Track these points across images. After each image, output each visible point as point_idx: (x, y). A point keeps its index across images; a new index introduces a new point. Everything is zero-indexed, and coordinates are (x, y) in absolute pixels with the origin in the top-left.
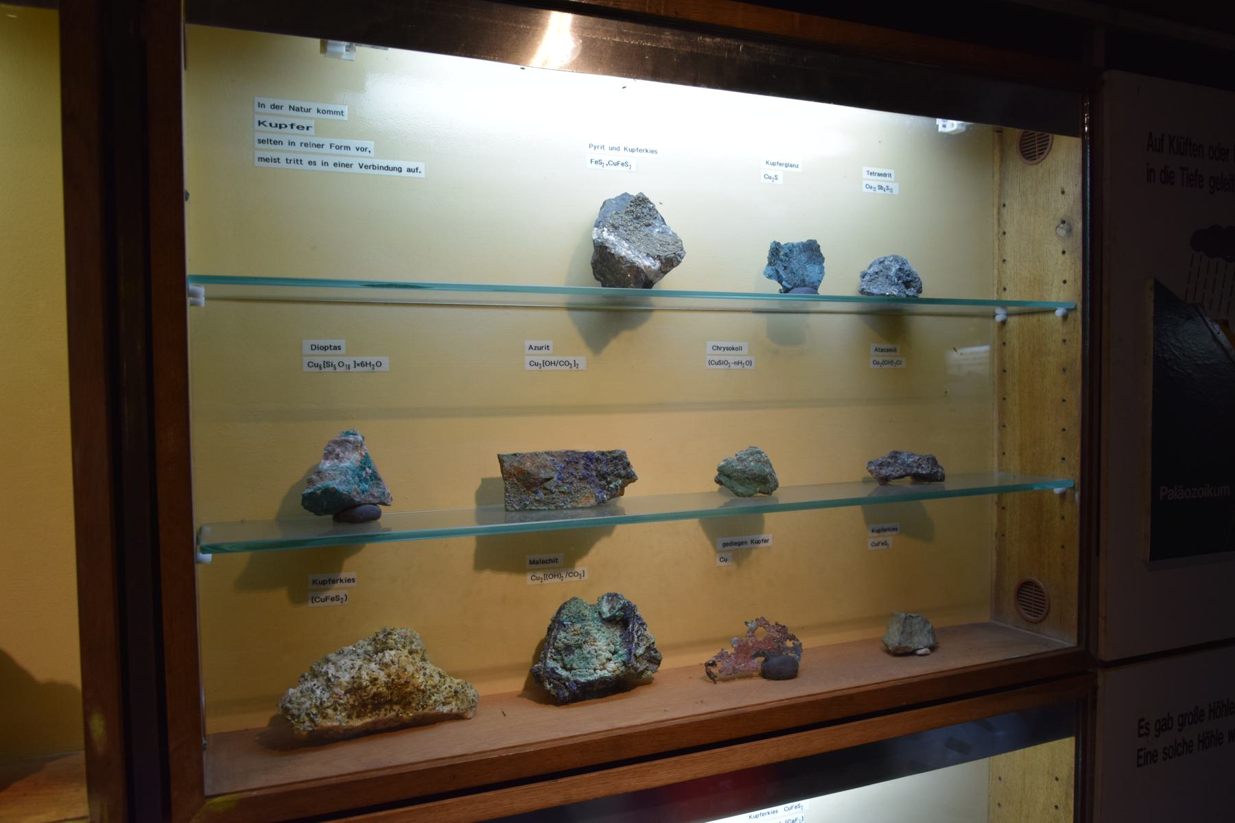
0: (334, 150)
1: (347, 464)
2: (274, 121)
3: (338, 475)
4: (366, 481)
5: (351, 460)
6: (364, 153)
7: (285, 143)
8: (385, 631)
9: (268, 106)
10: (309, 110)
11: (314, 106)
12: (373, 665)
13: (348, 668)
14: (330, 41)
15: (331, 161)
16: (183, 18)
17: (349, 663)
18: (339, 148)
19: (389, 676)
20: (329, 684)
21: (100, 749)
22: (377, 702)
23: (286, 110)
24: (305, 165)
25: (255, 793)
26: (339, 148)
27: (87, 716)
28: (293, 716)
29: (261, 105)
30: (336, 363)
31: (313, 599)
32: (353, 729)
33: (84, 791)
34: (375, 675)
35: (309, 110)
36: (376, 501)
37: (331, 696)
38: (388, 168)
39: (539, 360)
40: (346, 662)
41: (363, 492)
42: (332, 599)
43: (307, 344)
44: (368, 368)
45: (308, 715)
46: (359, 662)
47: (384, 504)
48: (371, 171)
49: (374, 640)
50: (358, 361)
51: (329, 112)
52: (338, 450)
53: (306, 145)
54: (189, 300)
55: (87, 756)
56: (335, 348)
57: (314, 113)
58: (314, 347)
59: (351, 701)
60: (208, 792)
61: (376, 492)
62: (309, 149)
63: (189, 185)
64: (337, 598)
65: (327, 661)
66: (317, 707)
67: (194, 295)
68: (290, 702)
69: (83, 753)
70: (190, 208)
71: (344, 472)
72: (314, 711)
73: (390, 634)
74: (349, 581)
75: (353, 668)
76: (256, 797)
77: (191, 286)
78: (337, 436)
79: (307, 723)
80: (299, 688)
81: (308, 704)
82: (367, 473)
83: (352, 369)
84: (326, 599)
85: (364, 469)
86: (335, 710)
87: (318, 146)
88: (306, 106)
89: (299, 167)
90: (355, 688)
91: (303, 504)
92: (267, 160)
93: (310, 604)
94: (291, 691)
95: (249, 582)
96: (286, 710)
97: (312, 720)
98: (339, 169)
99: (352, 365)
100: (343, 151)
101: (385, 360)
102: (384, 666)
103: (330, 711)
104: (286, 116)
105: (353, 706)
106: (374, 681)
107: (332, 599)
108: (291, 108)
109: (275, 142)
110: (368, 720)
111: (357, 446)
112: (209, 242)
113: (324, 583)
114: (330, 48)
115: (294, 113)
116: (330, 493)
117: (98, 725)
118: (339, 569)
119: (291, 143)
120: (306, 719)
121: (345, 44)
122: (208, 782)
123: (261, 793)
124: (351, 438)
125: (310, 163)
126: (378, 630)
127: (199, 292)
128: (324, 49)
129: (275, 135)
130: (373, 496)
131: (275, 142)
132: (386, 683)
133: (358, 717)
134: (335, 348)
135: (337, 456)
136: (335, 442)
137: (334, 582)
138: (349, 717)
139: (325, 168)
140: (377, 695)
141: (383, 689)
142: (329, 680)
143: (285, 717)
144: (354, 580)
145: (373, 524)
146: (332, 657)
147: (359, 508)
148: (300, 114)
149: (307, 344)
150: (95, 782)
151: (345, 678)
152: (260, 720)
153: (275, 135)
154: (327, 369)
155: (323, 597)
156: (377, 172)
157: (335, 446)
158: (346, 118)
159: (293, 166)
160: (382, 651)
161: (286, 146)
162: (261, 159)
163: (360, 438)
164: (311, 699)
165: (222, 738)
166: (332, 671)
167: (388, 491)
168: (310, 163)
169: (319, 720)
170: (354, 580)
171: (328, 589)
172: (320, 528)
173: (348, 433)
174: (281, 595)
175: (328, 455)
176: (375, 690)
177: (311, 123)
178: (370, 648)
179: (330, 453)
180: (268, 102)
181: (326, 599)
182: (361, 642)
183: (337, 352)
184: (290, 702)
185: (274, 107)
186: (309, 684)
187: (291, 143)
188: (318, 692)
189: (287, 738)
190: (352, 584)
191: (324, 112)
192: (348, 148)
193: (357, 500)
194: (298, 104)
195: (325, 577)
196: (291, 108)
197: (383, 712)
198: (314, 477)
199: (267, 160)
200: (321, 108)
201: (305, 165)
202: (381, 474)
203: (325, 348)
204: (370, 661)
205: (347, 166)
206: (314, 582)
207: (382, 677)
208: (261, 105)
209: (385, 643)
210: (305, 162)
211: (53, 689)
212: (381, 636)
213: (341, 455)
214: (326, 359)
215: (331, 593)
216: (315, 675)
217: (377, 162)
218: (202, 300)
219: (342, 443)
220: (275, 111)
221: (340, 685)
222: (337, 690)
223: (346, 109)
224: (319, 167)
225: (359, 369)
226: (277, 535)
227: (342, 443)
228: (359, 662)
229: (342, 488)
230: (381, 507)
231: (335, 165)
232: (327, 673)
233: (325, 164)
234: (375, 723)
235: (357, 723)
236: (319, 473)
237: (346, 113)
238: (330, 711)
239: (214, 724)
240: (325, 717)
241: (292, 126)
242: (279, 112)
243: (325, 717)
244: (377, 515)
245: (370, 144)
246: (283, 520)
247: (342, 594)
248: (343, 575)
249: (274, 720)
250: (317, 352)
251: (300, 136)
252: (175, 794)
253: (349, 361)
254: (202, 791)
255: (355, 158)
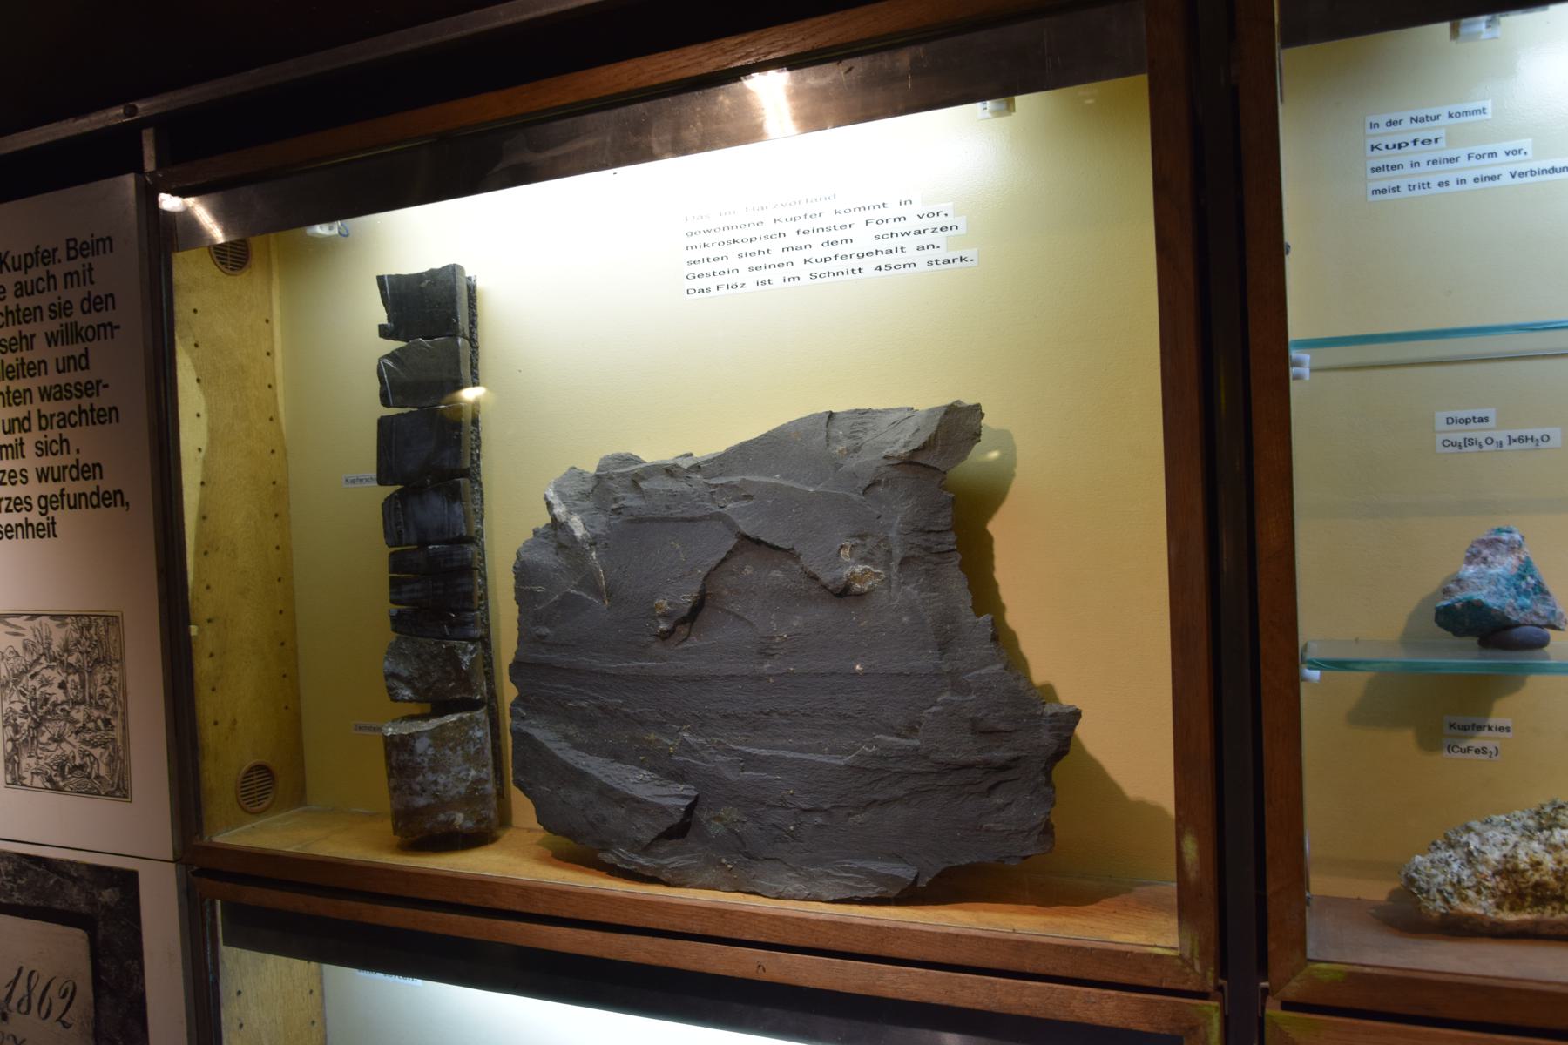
0: (1473, 161)
1: (1498, 570)
2: (1390, 141)
3: (1488, 584)
4: (1526, 593)
5: (1505, 565)
6: (1518, 157)
7: (1407, 165)
8: (1554, 803)
9: (1383, 124)
10: (1437, 117)
11: (1443, 111)
12: (1535, 845)
13: (1495, 843)
14: (1464, 21)
15: (1470, 176)
16: (1278, 44)
17: (1500, 837)
18: (1481, 156)
19: (1560, 862)
20: (1470, 859)
21: (1192, 875)
22: (1540, 895)
23: (1406, 124)
24: (1435, 189)
25: (1368, 970)
26: (1481, 156)
27: (1179, 835)
28: (1420, 889)
29: (1374, 125)
30: (1537, 436)
31: (1450, 748)
32: (1503, 924)
33: (1174, 923)
34: (1538, 857)
35: (1437, 117)
36: (1542, 622)
37: (1474, 874)
38: (1554, 170)
39: (1459, 438)
40: (1495, 835)
41: (1522, 608)
42: (1477, 751)
43: (1440, 417)
44: (1530, 444)
45: (1440, 892)
46: (1513, 838)
47: (1554, 627)
48: (1529, 179)
49: (1538, 813)
50: (1515, 435)
51: (1466, 113)
52: (1485, 552)
53: (1435, 162)
54: (1293, 370)
55: (1179, 888)
56: (1481, 420)
57: (1444, 120)
58: (1451, 421)
59: (1502, 886)
60: (1310, 955)
61: (1542, 609)
62: (1439, 167)
63: (1290, 236)
64: (1484, 750)
65: (1469, 829)
66: (1453, 885)
67: (1298, 364)
68: (1416, 871)
69: (1175, 885)
70: (1292, 264)
71: (1494, 581)
72: (1449, 889)
73: (1562, 807)
74: (1501, 729)
75: (1505, 843)
76: (1368, 974)
77: (1294, 354)
78: (1484, 535)
79: (1439, 903)
80: (1431, 856)
81: (1441, 878)
82: (1528, 582)
83: (1505, 446)
84: (1468, 750)
85: (1523, 578)
86: (1479, 893)
87: (1451, 160)
88: (1432, 112)
89: (1427, 191)
90: (1508, 870)
91: (1437, 619)
92: (1383, 191)
93: (1445, 753)
94: (1418, 858)
95: (1368, 714)
96: (1411, 881)
97: (1445, 900)
98: (1481, 185)
99: (1505, 441)
100: (1487, 161)
101: (1556, 433)
102: (1553, 848)
103: (1471, 893)
104: (1408, 131)
105: (1505, 894)
106: (1536, 865)
107: (1477, 751)
108: (1414, 120)
109: (1394, 167)
110: (1526, 916)
111: (1513, 548)
112: (1312, 302)
113: (1465, 728)
114: (1463, 31)
115: (1419, 125)
116: (1474, 607)
117: (1190, 847)
118: (1487, 712)
119: (1415, 164)
120: (1438, 896)
121: (1484, 19)
122: (1311, 945)
123: (1376, 971)
124: (1505, 537)
125: (1440, 184)
126: (1544, 801)
127: (1303, 363)
128: (1455, 33)
129: (1393, 158)
130: (1537, 614)
131: (1394, 167)
132: (1555, 872)
133: (1512, 909)
134: (1481, 420)
135: (1485, 561)
136: (1482, 542)
137: (1480, 728)
138: (1499, 906)
139: (1463, 187)
140: (1538, 885)
141: (1550, 879)
142: (1470, 853)
143: (1410, 889)
144: (1508, 730)
145: (1537, 652)
146: (1476, 825)
147: (1516, 630)
148: (1426, 124)
149: (1440, 417)
150: (1186, 910)
151: (1495, 855)
152: (1378, 891)
153: (1393, 158)
154: (1470, 448)
155: (1464, 746)
156: (1537, 178)
157: (1481, 548)
158: (1489, 116)
159: (1417, 192)
160: (1550, 828)
161: (1407, 169)
162: (1375, 192)
163: (1517, 537)
164: (1445, 873)
165: (1329, 902)
166: (1474, 843)
167: (1560, 610)
168: (1440, 184)
169: (1455, 902)
170: (1508, 730)
171: (1466, 738)
172: (1464, 656)
173: (1500, 531)
174: (1408, 736)
175: (1471, 558)
176: (1537, 877)
177: (1442, 133)
178: (1531, 823)
179: (1475, 556)
180: (1382, 119)
181: (1468, 750)
182: (1518, 813)
183: (1483, 425)
184: (1416, 871)
185: (1391, 123)
186: (1443, 854)
187: (1415, 164)
188: (1455, 866)
189: (1409, 916)
190: (1505, 734)
191: (1458, 115)
192: (1493, 154)
193: (1514, 618)
194: (1421, 113)
195: (1469, 720)
196: (1414, 120)
197: (1549, 910)
198: (1452, 586)
199: (1383, 191)
200: (1453, 111)
201: (1435, 189)
202: (1549, 586)
203: (1466, 421)
204: (1531, 839)
205: (1492, 178)
206: (1451, 726)
207: (1549, 862)
208: (1374, 125)
209: (1555, 819)
210: (1434, 184)
211: (1142, 809)
212: (1548, 810)
213: (1490, 559)
214: (1469, 435)
215: (1475, 743)
216: (1451, 845)
217: (1535, 166)
218: (1306, 371)
219: (1492, 543)
220: (1393, 128)
221: (1486, 862)
222: (1481, 868)
223: (1488, 105)
224: (1453, 187)
225: (1516, 446)
226: (1401, 656)
227: (1492, 543)
228: (1513, 838)
229: (1492, 602)
230: (1550, 632)
231: (1476, 180)
232: (1467, 844)
233: (1462, 181)
234: (1536, 923)
235: (1510, 917)
236: (1459, 581)
237: (1489, 110)
238: (1471, 893)
239: (1319, 884)
240: (1464, 899)
241: (1415, 142)
242: (1397, 128)
243: (1464, 899)
244: (1542, 643)
245: (1525, 143)
246: (1409, 639)
247: (1490, 746)
248: (1493, 721)
249: (1394, 894)
250: (1455, 426)
251: (1423, 154)
252: (1272, 946)
253: (1500, 436)
254: (1304, 952)
255: (1502, 166)
